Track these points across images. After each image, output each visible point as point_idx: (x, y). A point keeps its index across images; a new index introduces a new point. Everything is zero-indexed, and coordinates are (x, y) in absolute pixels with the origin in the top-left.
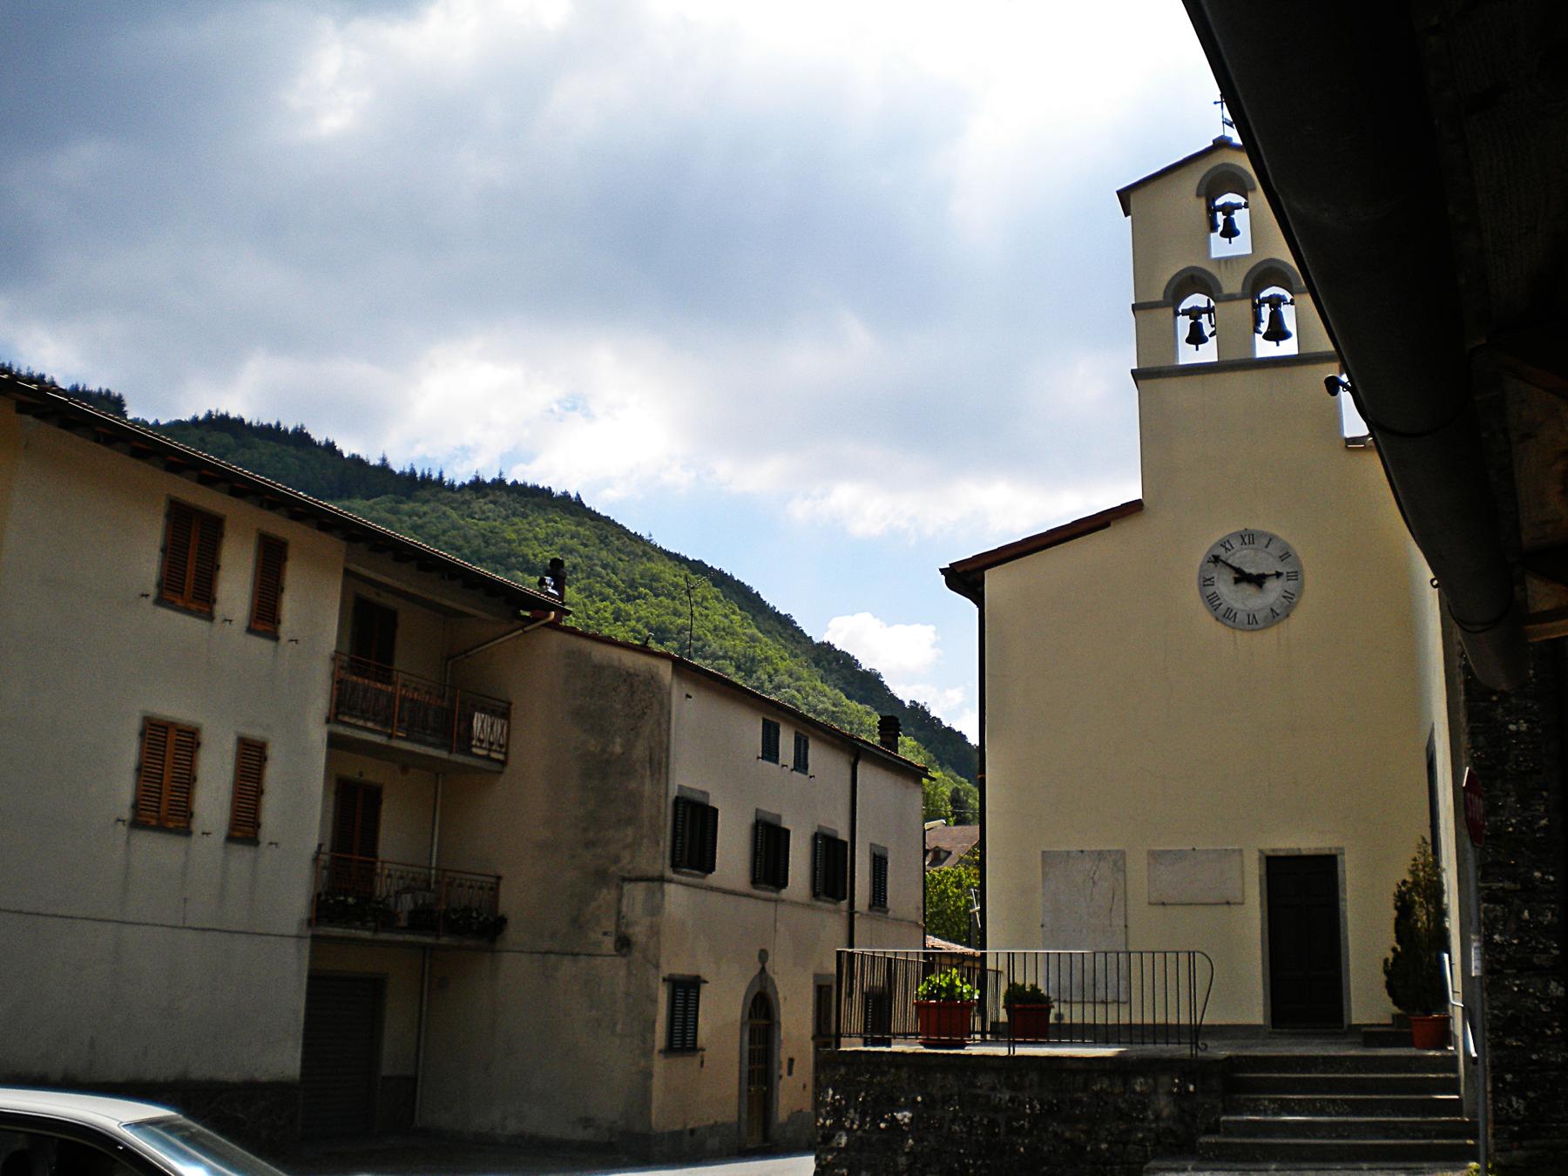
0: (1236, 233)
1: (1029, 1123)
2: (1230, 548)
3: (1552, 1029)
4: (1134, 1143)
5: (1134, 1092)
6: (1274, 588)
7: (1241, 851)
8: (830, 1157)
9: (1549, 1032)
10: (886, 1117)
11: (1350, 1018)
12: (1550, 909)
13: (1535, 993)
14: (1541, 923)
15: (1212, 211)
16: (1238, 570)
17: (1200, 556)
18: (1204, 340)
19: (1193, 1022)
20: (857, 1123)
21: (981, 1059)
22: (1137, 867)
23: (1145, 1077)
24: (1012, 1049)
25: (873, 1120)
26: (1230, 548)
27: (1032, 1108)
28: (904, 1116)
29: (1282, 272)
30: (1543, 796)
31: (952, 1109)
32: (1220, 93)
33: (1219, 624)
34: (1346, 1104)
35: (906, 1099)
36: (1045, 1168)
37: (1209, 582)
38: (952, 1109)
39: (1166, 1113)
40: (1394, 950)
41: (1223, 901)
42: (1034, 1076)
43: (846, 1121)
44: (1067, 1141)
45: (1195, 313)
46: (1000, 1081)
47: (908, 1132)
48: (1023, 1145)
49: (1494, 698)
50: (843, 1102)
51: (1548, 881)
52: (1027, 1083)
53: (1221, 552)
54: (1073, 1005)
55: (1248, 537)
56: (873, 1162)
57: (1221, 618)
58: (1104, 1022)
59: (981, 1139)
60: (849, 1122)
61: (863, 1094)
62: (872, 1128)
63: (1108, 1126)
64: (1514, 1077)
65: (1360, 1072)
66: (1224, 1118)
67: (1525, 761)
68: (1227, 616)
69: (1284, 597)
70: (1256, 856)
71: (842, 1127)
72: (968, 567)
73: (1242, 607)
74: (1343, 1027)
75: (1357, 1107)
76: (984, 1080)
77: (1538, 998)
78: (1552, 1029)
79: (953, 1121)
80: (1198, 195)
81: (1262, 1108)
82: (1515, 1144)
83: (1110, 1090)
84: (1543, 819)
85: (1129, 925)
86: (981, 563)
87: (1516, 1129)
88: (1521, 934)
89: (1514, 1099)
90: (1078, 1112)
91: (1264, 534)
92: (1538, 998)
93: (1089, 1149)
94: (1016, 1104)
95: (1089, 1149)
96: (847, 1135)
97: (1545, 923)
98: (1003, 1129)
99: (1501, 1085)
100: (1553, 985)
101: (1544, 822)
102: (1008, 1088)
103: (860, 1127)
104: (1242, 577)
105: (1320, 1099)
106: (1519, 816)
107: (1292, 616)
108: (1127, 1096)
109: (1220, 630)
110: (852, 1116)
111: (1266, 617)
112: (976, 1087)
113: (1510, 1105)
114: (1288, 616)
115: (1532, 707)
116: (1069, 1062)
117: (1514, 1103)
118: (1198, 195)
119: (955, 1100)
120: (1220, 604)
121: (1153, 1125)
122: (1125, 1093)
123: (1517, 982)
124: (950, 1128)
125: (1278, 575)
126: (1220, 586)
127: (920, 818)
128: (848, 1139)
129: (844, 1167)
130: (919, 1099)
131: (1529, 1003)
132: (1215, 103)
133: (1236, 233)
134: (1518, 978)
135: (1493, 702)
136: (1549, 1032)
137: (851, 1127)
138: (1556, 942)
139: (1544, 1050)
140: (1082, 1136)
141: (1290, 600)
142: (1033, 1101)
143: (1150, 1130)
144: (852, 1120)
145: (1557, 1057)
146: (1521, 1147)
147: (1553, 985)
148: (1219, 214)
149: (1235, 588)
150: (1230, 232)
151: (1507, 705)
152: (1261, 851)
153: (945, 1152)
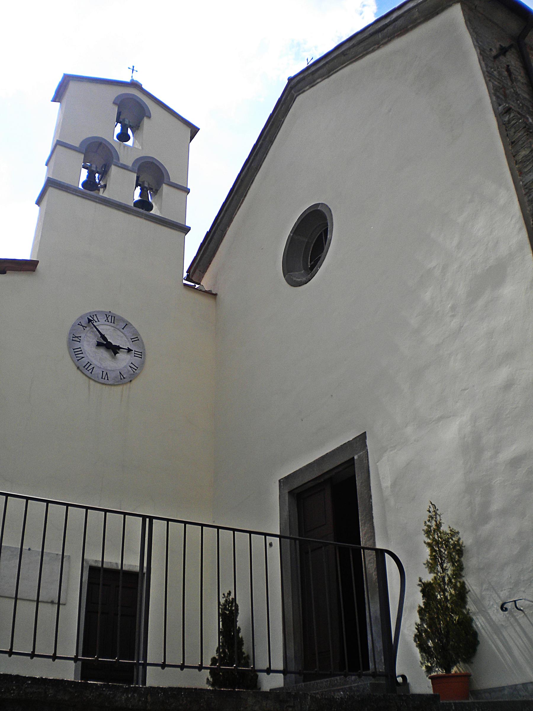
2: (97, 320)
6: (124, 359)
11: (76, 666)
37: (76, 339)
41: (50, 601)
55: (111, 318)
69: (131, 367)
73: (99, 365)
80: (114, 103)
91: (122, 320)
107: (133, 382)
111: (116, 377)
118: (114, 103)
120: (83, 357)
125: (129, 350)
132: (133, 67)
149: (96, 350)
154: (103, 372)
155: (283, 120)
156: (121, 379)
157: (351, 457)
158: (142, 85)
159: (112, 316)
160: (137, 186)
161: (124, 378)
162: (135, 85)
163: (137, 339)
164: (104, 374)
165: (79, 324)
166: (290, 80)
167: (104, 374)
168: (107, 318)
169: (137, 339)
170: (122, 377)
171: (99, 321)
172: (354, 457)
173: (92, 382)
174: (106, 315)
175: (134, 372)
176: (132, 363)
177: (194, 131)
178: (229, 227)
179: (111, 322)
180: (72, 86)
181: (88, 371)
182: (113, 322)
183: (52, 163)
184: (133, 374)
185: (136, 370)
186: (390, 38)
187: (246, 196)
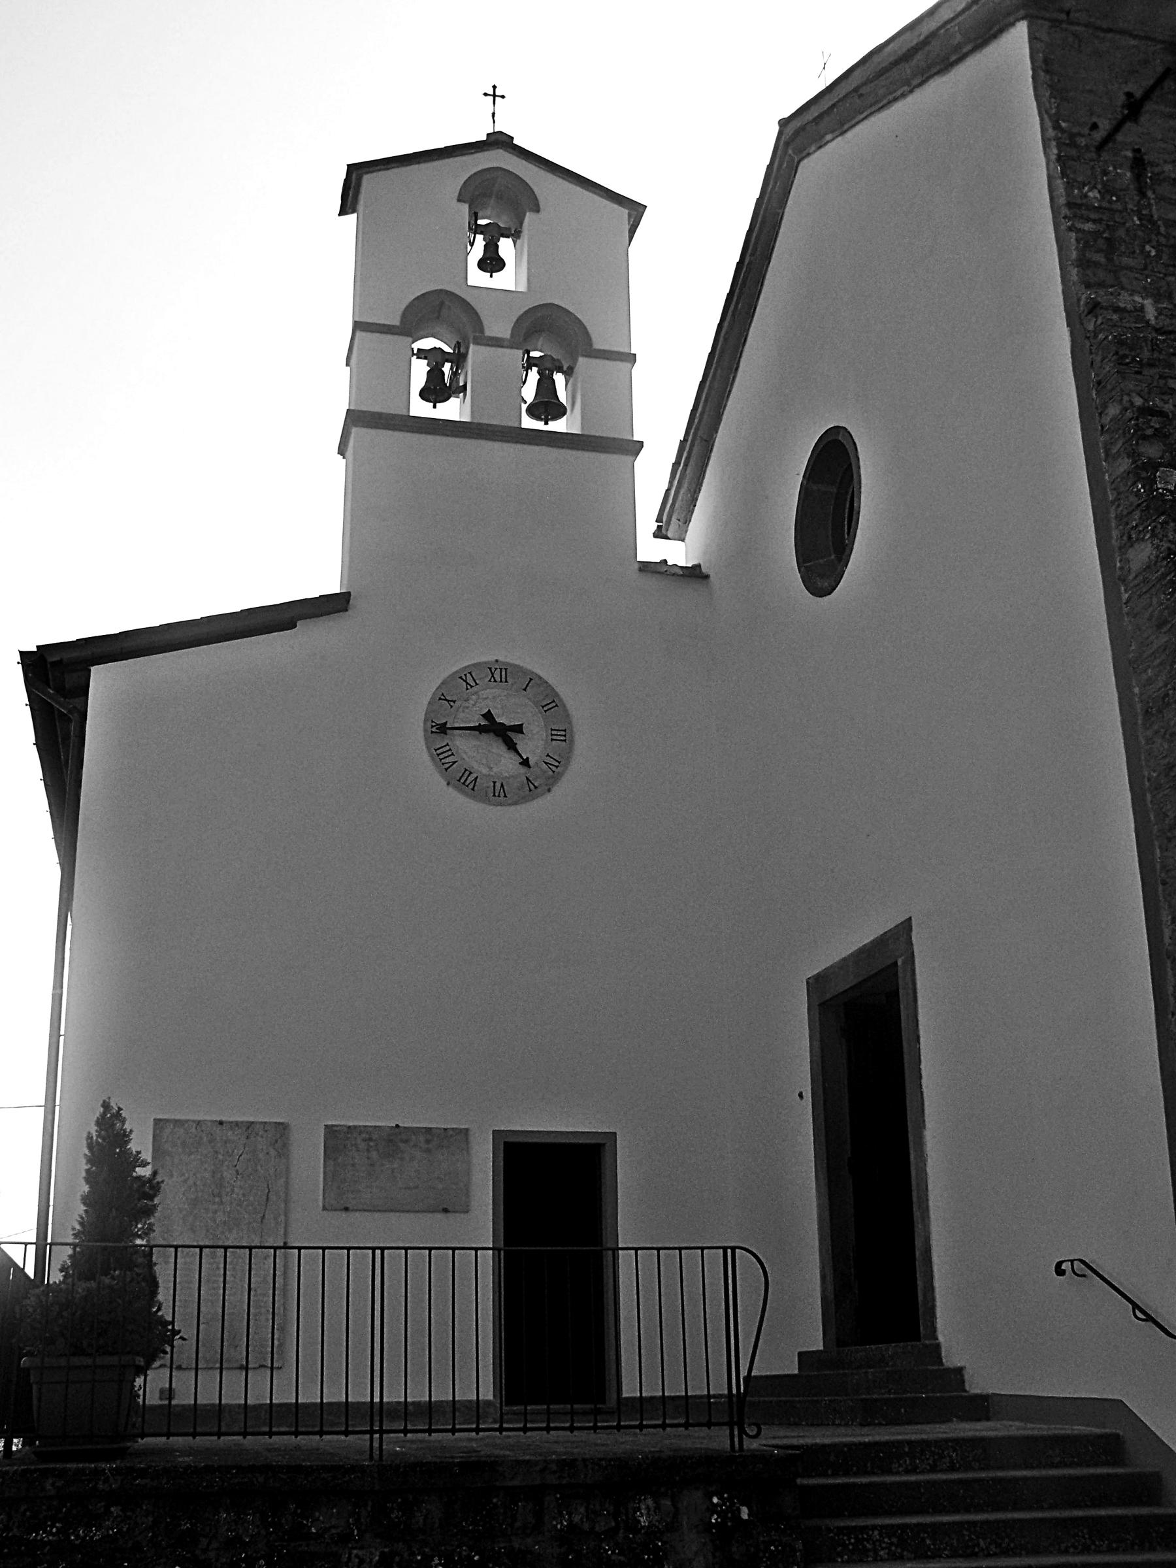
2: (473, 684)
5: (634, 1526)
26: (473, 684)
32: (728, 292)
52: (129, 1514)
69: (546, 763)
72: (66, 656)
86: (87, 653)
114: (549, 790)
126: (458, 743)
132: (494, 87)
154: (494, 783)
155: (781, 211)
156: (530, 790)
157: (890, 962)
158: (512, 138)
159: (501, 669)
160: (528, 368)
161: (536, 787)
162: (499, 141)
163: (554, 704)
164: (498, 785)
165: (440, 699)
166: (783, 123)
167: (498, 785)
168: (493, 674)
169: (554, 704)
170: (532, 786)
171: (477, 684)
172: (896, 963)
174: (490, 669)
175: (554, 772)
176: (548, 755)
177: (636, 210)
178: (717, 432)
179: (501, 681)
180: (368, 181)
181: (467, 786)
182: (503, 680)
183: (353, 361)
184: (553, 777)
185: (557, 767)
186: (925, 75)
187: (737, 369)
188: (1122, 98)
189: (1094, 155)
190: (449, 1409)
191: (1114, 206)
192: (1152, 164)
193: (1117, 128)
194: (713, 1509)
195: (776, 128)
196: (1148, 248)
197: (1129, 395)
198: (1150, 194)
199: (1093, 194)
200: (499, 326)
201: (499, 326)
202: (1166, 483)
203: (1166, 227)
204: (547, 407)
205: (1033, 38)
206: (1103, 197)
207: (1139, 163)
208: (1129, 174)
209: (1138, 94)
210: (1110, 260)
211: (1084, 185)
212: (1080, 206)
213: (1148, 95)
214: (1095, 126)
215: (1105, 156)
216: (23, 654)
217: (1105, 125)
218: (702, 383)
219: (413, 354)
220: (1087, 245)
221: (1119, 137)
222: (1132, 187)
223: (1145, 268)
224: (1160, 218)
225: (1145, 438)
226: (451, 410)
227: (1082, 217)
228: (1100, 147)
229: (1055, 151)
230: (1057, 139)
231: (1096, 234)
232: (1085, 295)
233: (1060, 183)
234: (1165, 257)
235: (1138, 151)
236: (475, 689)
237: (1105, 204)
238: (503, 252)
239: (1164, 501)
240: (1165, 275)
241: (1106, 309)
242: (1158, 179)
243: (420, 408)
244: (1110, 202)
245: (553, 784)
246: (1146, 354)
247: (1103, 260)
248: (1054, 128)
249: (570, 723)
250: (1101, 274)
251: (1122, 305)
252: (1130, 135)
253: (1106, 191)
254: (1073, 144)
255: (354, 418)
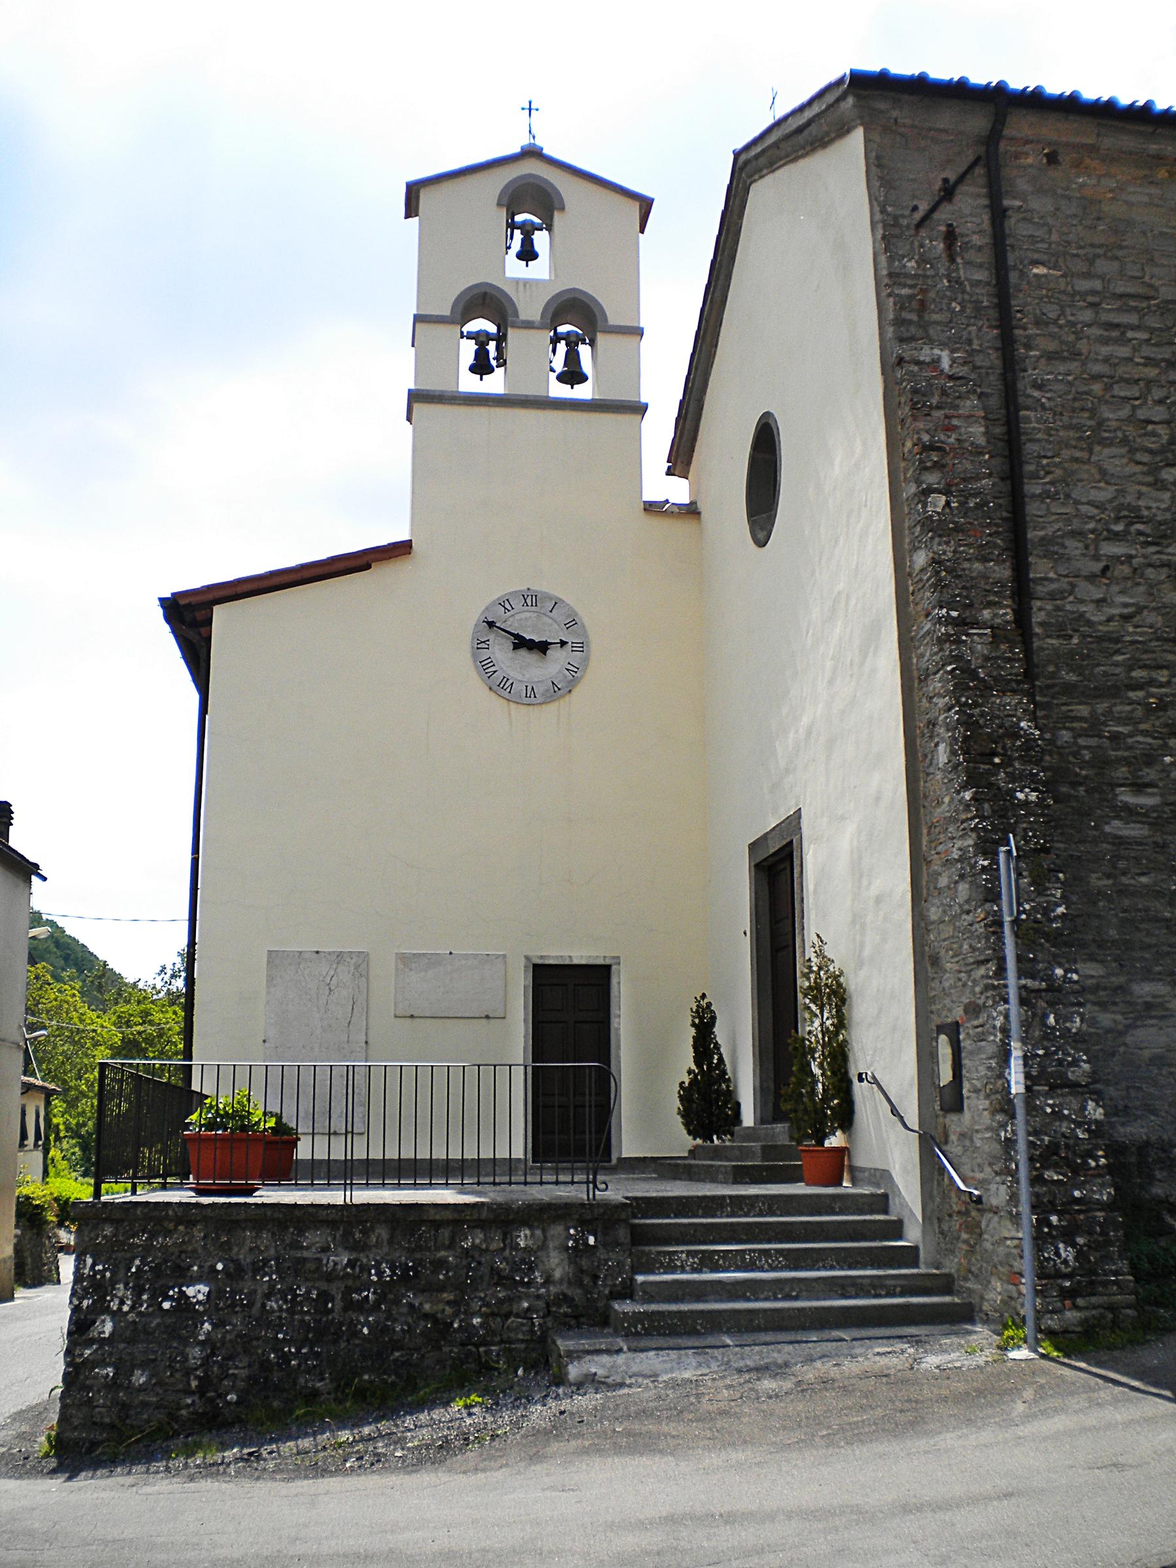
0: (534, 256)
1: (374, 1293)
3: (1096, 1159)
4: (518, 1316)
5: (516, 1247)
7: (504, 956)
8: (88, 1352)
9: (1093, 1164)
10: (171, 1293)
12: (1080, 1014)
13: (1070, 1114)
14: (1069, 1030)
15: (512, 226)
16: (517, 636)
17: (473, 615)
18: (490, 370)
19: (349, 1157)
20: (129, 1302)
21: (311, 1210)
22: (383, 971)
23: (531, 1227)
24: (348, 1193)
25: (153, 1298)
27: (380, 1274)
28: (197, 1292)
29: (588, 306)
30: (1058, 878)
31: (267, 1278)
33: (493, 694)
34: (781, 1255)
35: (200, 1267)
36: (397, 1354)
38: (267, 1278)
39: (557, 1274)
40: (690, 1072)
42: (383, 1232)
43: (112, 1300)
44: (426, 1316)
45: (481, 339)
46: (334, 1238)
47: (205, 1312)
48: (367, 1324)
49: (997, 760)
50: (108, 1274)
51: (1071, 981)
53: (498, 615)
54: (316, 1137)
55: (531, 598)
56: (152, 1357)
57: (495, 687)
58: (428, 1157)
59: (307, 1318)
60: (117, 1301)
61: (137, 1262)
62: (151, 1309)
63: (482, 1295)
64: (1060, 1220)
65: (773, 1214)
66: (640, 1278)
67: (1034, 836)
68: (501, 687)
70: (522, 963)
71: (107, 1311)
72: (193, 600)
73: (520, 677)
74: (610, 1161)
75: (796, 1260)
76: (314, 1238)
77: (1074, 1121)
78: (1096, 1159)
79: (268, 1296)
80: (499, 204)
81: (678, 1264)
82: (1068, 1303)
83: (484, 1246)
84: (1060, 906)
85: (371, 1041)
86: (210, 596)
87: (1068, 1284)
88: (1045, 1043)
89: (1061, 1246)
90: (441, 1277)
91: (550, 598)
92: (1074, 1121)
93: (456, 1325)
94: (357, 1269)
95: (456, 1325)
96: (112, 1320)
97: (1074, 1030)
98: (339, 1304)
99: (1046, 1230)
100: (1091, 1105)
101: (1061, 910)
102: (346, 1248)
103: (133, 1308)
104: (521, 643)
105: (750, 1250)
106: (1033, 901)
107: (575, 692)
108: (507, 1252)
109: (495, 703)
110: (120, 1294)
112: (302, 1248)
113: (1058, 1254)
115: (1037, 774)
116: (432, 1212)
117: (1062, 1251)
119: (271, 1267)
121: (543, 1290)
122: (504, 1249)
123: (1051, 1102)
124: (264, 1305)
125: (563, 643)
127: (27, 923)
128: (114, 1327)
129: (109, 1365)
130: (220, 1266)
131: (1064, 1128)
133: (534, 256)
134: (1052, 1098)
135: (995, 765)
136: (1093, 1164)
137: (120, 1309)
138: (1085, 1054)
139: (1088, 1187)
140: (447, 1308)
141: (574, 675)
142: (381, 1263)
143: (538, 1297)
144: (122, 1298)
145: (1101, 1194)
146: (1076, 1307)
147: (1091, 1105)
148: (517, 232)
150: (528, 254)
151: (1009, 770)
152: (527, 958)
153: (258, 1339)
162: (532, 153)
164: (529, 689)
167: (529, 689)
173: (513, 705)
177: (645, 205)
188: (938, 184)
189: (912, 232)
190: (475, 1164)
191: (928, 273)
192: (962, 236)
193: (933, 210)
194: (570, 1237)
195: (732, 157)
196: (954, 304)
197: (918, 433)
198: (959, 260)
199: (912, 264)
200: (531, 308)
201: (531, 308)
202: (935, 506)
203: (972, 286)
204: (573, 375)
205: (867, 141)
206: (919, 267)
207: (950, 236)
208: (942, 245)
209: (953, 178)
210: (920, 317)
211: (904, 257)
212: (898, 275)
213: (961, 179)
214: (915, 208)
215: (923, 233)
216: (161, 600)
217: (923, 207)
218: (693, 355)
219: (462, 337)
220: (902, 308)
221: (936, 216)
222: (944, 255)
223: (950, 322)
224: (967, 279)
225: (926, 469)
226: (494, 383)
227: (900, 284)
228: (920, 225)
229: (881, 232)
230: (883, 221)
231: (911, 297)
232: (898, 350)
233: (883, 259)
234: (968, 311)
235: (951, 225)
236: (512, 612)
237: (920, 272)
238: (537, 247)
239: (932, 521)
240: (968, 325)
241: (909, 362)
242: (966, 246)
243: (469, 383)
244: (925, 269)
245: (574, 686)
246: (935, 401)
247: (915, 318)
248: (881, 212)
249: (587, 637)
250: (913, 330)
251: (922, 359)
252: (944, 214)
253: (922, 261)
254: (896, 224)
255: (416, 397)
